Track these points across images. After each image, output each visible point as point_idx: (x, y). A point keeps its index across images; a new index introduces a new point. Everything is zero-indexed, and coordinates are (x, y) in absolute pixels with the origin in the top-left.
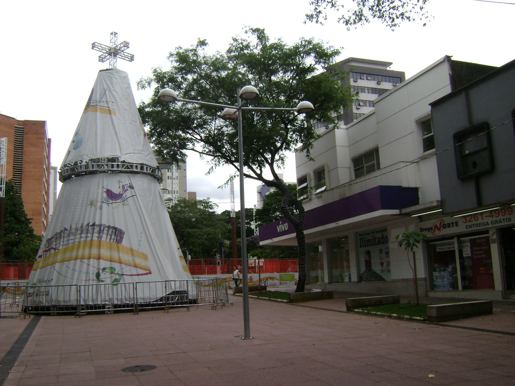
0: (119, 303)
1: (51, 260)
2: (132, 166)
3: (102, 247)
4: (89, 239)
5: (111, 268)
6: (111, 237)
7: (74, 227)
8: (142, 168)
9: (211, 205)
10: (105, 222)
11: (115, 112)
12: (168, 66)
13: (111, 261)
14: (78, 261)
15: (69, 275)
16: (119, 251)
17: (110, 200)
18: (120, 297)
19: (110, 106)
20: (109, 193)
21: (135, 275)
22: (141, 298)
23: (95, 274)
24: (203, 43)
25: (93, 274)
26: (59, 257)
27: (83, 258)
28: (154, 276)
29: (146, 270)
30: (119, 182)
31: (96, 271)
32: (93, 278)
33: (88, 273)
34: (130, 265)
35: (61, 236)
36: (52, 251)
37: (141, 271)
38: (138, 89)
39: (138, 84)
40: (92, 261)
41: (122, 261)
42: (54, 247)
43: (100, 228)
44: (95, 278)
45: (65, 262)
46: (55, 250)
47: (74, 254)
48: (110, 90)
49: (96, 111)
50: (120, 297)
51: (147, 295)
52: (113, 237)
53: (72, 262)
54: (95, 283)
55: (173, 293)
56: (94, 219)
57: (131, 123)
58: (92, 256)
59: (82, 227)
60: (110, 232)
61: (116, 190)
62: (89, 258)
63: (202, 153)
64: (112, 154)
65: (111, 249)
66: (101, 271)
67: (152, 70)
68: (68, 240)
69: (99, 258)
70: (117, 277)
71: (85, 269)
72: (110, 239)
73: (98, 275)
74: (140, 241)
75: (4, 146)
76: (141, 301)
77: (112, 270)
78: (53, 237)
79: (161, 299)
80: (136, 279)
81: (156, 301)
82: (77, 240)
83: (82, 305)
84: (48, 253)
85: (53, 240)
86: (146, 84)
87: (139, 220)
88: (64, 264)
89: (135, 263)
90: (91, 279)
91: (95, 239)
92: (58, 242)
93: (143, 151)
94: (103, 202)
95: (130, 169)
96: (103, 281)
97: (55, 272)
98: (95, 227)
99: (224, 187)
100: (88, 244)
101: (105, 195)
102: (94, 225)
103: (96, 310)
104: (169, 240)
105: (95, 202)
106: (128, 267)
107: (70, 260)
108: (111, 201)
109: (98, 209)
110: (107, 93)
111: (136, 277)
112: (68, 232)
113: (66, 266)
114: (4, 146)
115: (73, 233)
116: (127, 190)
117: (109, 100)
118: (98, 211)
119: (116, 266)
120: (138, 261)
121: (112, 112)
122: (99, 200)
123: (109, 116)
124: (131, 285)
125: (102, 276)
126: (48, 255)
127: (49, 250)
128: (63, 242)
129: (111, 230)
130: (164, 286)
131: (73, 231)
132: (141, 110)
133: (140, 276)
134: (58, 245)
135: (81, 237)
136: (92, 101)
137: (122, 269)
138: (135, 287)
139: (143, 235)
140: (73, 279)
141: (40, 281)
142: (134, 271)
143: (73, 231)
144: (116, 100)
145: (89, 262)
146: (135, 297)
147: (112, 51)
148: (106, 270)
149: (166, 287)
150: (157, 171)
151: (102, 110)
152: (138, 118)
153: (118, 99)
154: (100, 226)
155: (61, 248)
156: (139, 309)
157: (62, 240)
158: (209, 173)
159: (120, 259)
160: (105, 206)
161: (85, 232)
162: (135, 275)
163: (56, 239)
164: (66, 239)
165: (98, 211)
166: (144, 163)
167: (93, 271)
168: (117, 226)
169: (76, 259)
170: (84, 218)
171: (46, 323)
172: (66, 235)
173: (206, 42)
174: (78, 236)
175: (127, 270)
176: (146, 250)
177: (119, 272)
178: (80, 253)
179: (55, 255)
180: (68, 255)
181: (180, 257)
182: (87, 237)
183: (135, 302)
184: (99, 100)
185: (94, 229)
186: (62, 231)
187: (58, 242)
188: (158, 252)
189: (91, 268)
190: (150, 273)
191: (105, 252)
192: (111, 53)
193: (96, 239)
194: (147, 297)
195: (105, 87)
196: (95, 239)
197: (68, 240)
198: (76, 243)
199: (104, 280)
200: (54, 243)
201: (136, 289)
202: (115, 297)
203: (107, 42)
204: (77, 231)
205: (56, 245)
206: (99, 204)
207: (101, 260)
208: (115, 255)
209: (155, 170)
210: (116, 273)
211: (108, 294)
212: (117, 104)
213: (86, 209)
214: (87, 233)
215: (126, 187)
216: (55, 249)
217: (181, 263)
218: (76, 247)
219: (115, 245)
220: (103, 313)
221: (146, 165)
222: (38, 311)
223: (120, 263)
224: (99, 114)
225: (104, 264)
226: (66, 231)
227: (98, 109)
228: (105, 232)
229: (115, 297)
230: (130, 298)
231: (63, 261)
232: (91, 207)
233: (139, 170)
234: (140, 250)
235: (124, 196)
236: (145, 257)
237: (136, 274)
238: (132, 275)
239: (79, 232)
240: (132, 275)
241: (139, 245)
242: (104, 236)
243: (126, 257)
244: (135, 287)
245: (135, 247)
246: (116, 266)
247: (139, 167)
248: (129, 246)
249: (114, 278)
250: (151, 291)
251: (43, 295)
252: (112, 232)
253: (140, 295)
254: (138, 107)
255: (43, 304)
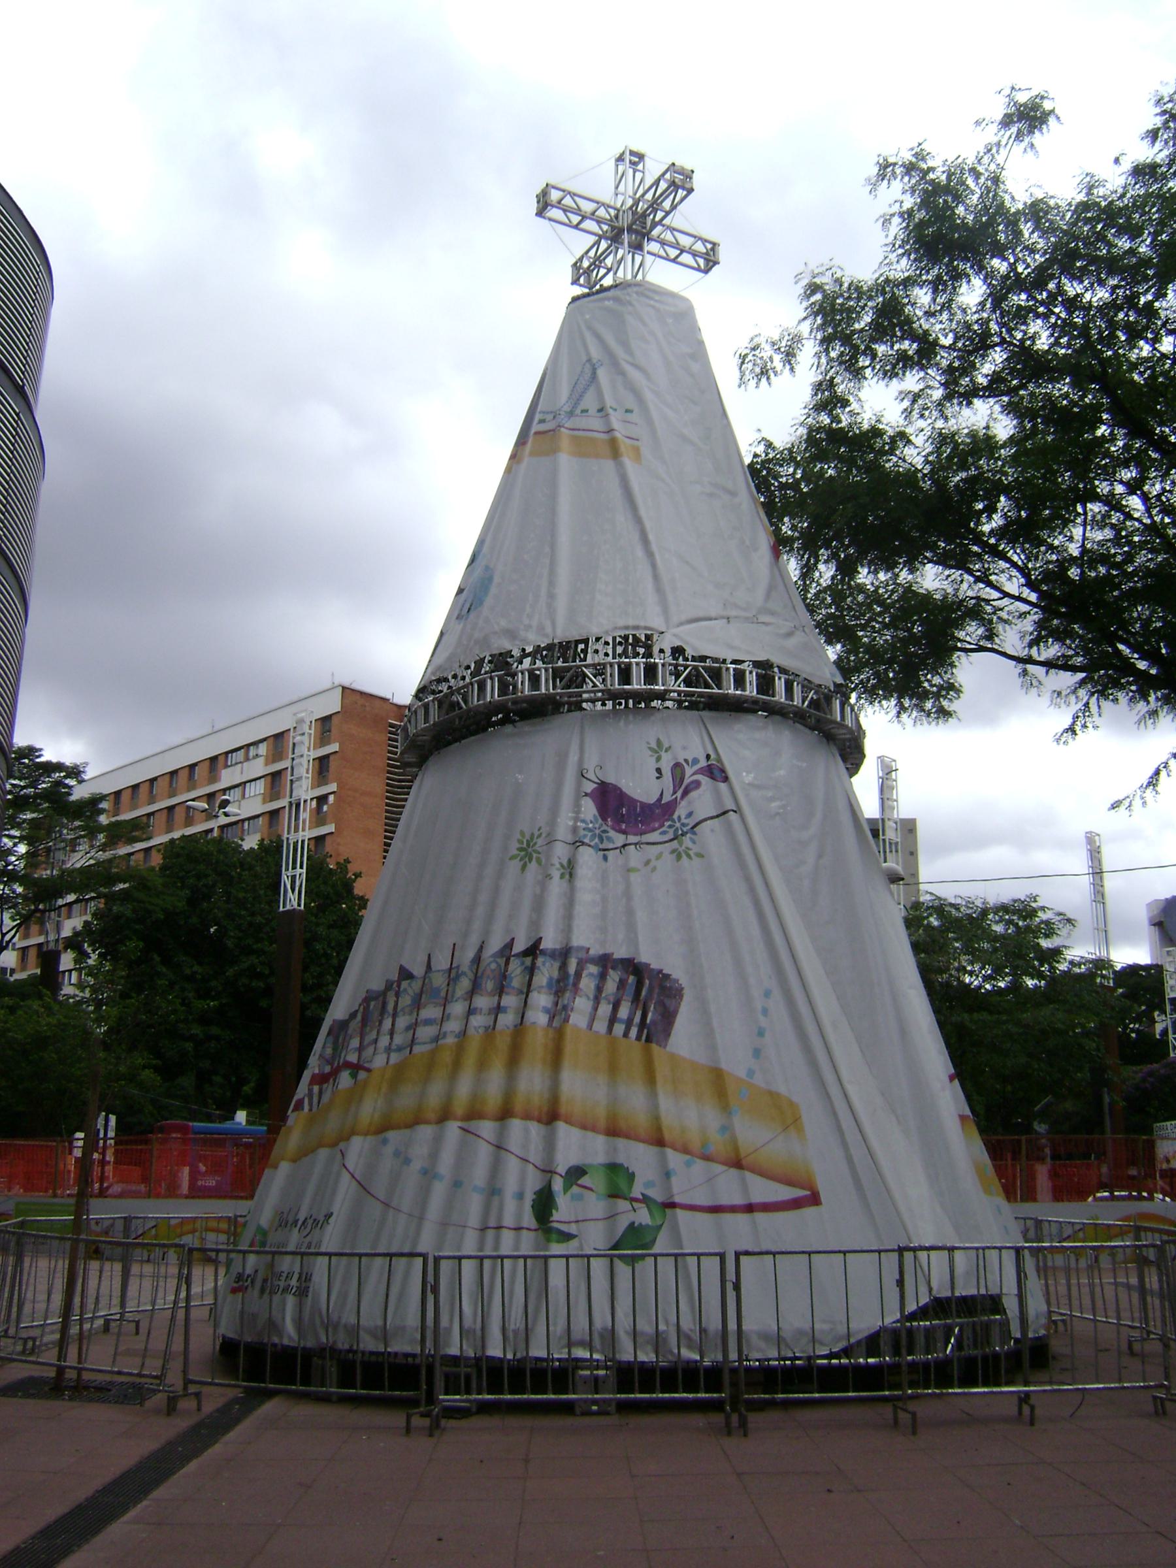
0: (646, 1356)
1: (332, 1124)
2: (716, 675)
3: (566, 1064)
4: (507, 1020)
5: (613, 1168)
6: (616, 1006)
7: (442, 962)
8: (765, 684)
9: (1047, 923)
10: (584, 937)
11: (637, 450)
12: (869, 251)
13: (613, 1131)
14: (453, 1129)
15: (406, 1199)
16: (650, 1078)
17: (612, 833)
18: (645, 1326)
19: (616, 425)
20: (612, 802)
21: (733, 1209)
22: (765, 1337)
23: (529, 1197)
24: (1029, 117)
25: (520, 1196)
26: (370, 1109)
27: (474, 1114)
28: (834, 1222)
29: (789, 1182)
30: (658, 749)
31: (533, 1183)
32: (519, 1215)
33: (493, 1191)
34: (707, 1158)
35: (384, 1004)
36: (345, 1079)
37: (764, 1190)
38: (742, 382)
39: (743, 358)
40: (516, 1124)
41: (667, 1136)
42: (353, 1058)
43: (563, 967)
44: (529, 1220)
45: (391, 1135)
46: (354, 1076)
47: (435, 1094)
48: (615, 363)
49: (554, 450)
50: (645, 1326)
51: (795, 1319)
52: (623, 1012)
53: (425, 1132)
54: (527, 1244)
55: (939, 1307)
56: (536, 923)
57: (711, 495)
58: (519, 1105)
59: (477, 959)
60: (611, 986)
61: (643, 787)
62: (505, 1114)
63: (1029, 660)
64: (621, 623)
65: (613, 1069)
66: (558, 1185)
67: (799, 289)
68: (413, 1027)
69: (551, 1116)
70: (643, 1216)
71: (479, 1174)
72: (613, 1020)
73: (544, 1204)
74: (761, 1033)
75: (306, 738)
76: (761, 1353)
77: (618, 1179)
78: (353, 1015)
79: (872, 1343)
80: (740, 1231)
81: (846, 1352)
82: (453, 1026)
83: (455, 1360)
84: (328, 1088)
85: (355, 1025)
86: (777, 358)
87: (755, 931)
88: (385, 1142)
89: (736, 1149)
90: (508, 1220)
91: (538, 1018)
92: (373, 1035)
93: (772, 613)
94: (577, 843)
95: (711, 693)
96: (567, 1237)
97: (346, 1177)
98: (540, 960)
99: (1137, 803)
100: (503, 1042)
101: (589, 809)
102: (533, 951)
103: (527, 1387)
104: (903, 1032)
105: (540, 842)
106: (699, 1165)
107: (416, 1121)
108: (620, 839)
109: (556, 874)
110: (601, 373)
111: (742, 1218)
112: (416, 985)
113: (397, 1154)
114: (306, 738)
115: (438, 990)
116: (697, 784)
117: (609, 402)
118: (557, 886)
119: (639, 1157)
120: (753, 1134)
121: (623, 449)
122: (563, 831)
123: (609, 465)
124: (711, 1266)
125: (564, 1210)
126: (326, 1098)
127: (335, 1073)
128: (392, 1033)
129: (614, 977)
130: (890, 1276)
131: (439, 981)
132: (760, 475)
133: (760, 1217)
134: (371, 1050)
135: (471, 1012)
136: (537, 417)
137: (667, 1175)
138: (731, 1275)
139: (777, 1004)
140: (421, 1218)
141: (284, 1221)
142: (730, 1187)
143: (439, 981)
144: (640, 400)
145: (502, 1134)
146: (732, 1325)
147: (625, 220)
148: (584, 1181)
149: (900, 1283)
150: (837, 704)
151: (583, 447)
152: (747, 499)
153: (649, 396)
154: (564, 954)
155: (379, 1061)
156: (748, 1402)
157: (387, 1023)
158: (1071, 730)
159: (656, 1119)
160: (587, 858)
161: (489, 985)
162: (733, 1209)
163: (364, 1022)
164: (402, 1022)
165: (557, 886)
166: (776, 659)
167: (520, 1182)
168: (645, 956)
169: (444, 1116)
170: (490, 918)
171: (287, 1436)
172: (406, 1001)
173: (1047, 105)
174: (458, 1008)
175: (691, 1181)
176: (788, 1077)
177: (654, 1193)
178: (464, 1089)
179: (355, 1096)
180: (406, 1100)
181: (962, 1118)
182: (498, 1009)
183: (733, 1356)
184: (567, 408)
185: (531, 971)
186: (389, 985)
187: (373, 1035)
188: (851, 1090)
189: (512, 1166)
190: (814, 1199)
191: (580, 1086)
192: (621, 231)
193: (542, 1019)
194: (800, 1332)
195: (595, 353)
196: (538, 1018)
197: (413, 1027)
198: (450, 1040)
199: (572, 1229)
200: (355, 1043)
201: (737, 1287)
202: (624, 1322)
203: (602, 186)
204: (458, 977)
205: (361, 1049)
206: (561, 852)
207: (561, 1126)
208: (634, 1102)
209: (828, 699)
210: (636, 1192)
211: (595, 1309)
212: (650, 422)
213: (500, 874)
214: (501, 991)
215: (689, 771)
216: (355, 1068)
217: (965, 1150)
218: (447, 1057)
219: (632, 1049)
220: (567, 1408)
221: (783, 671)
222: (262, 1367)
223: (660, 1142)
224: (565, 461)
225: (573, 1146)
226: (404, 984)
227: (565, 443)
228: (587, 984)
229: (624, 1322)
230: (703, 1331)
231: (383, 1128)
232: (524, 868)
233: (751, 690)
234: (759, 1080)
235: (681, 811)
236: (785, 1115)
237: (738, 1200)
238: (716, 1209)
239: (465, 984)
240: (716, 1209)
241: (757, 1053)
242: (582, 1004)
243: (688, 1115)
244: (731, 1275)
245: (736, 1062)
246: (639, 1157)
247: (751, 679)
248: (700, 1056)
249: (623, 1224)
250: (815, 1296)
251: (286, 1289)
252: (622, 984)
253: (757, 1317)
254: (747, 460)
255: (280, 1335)
